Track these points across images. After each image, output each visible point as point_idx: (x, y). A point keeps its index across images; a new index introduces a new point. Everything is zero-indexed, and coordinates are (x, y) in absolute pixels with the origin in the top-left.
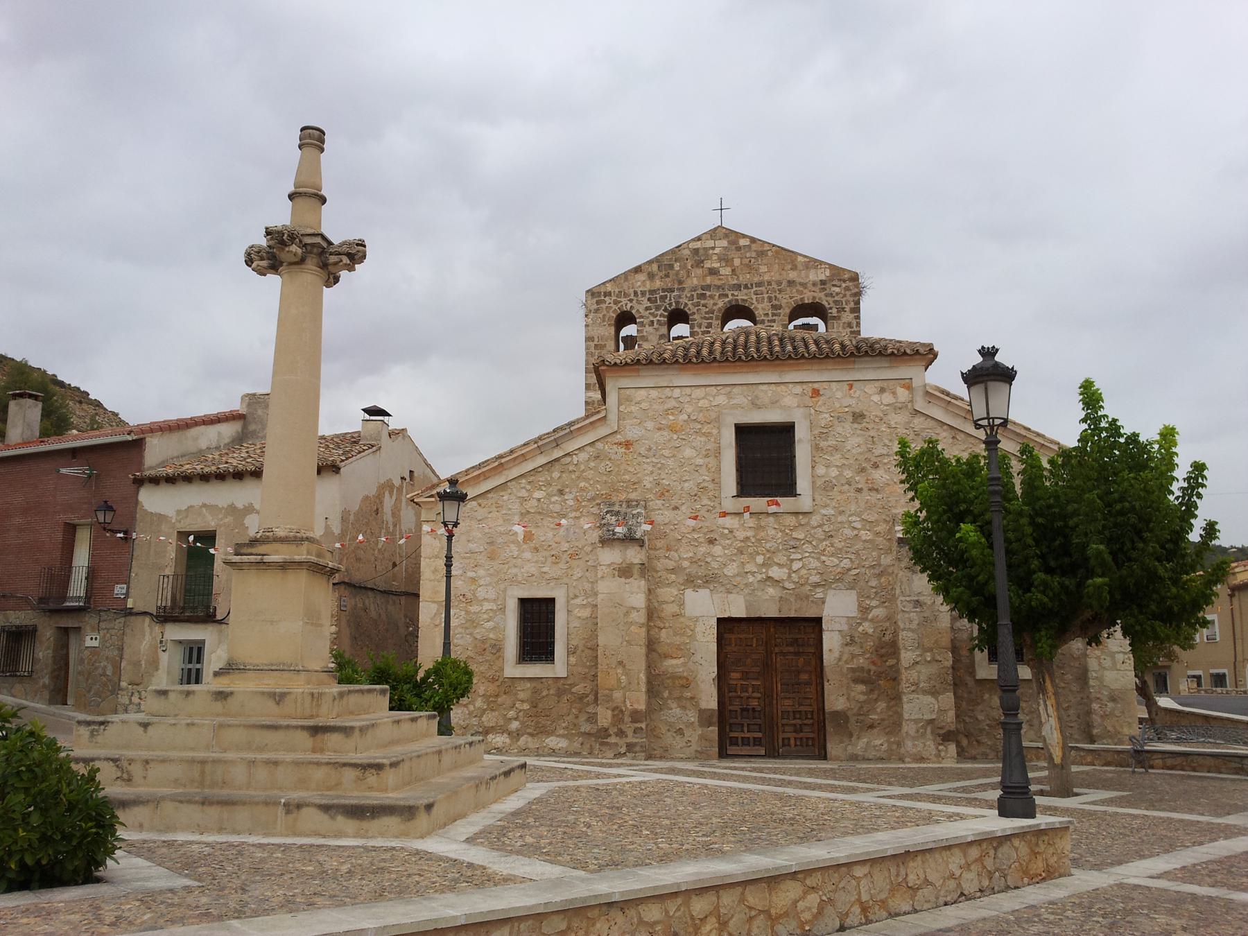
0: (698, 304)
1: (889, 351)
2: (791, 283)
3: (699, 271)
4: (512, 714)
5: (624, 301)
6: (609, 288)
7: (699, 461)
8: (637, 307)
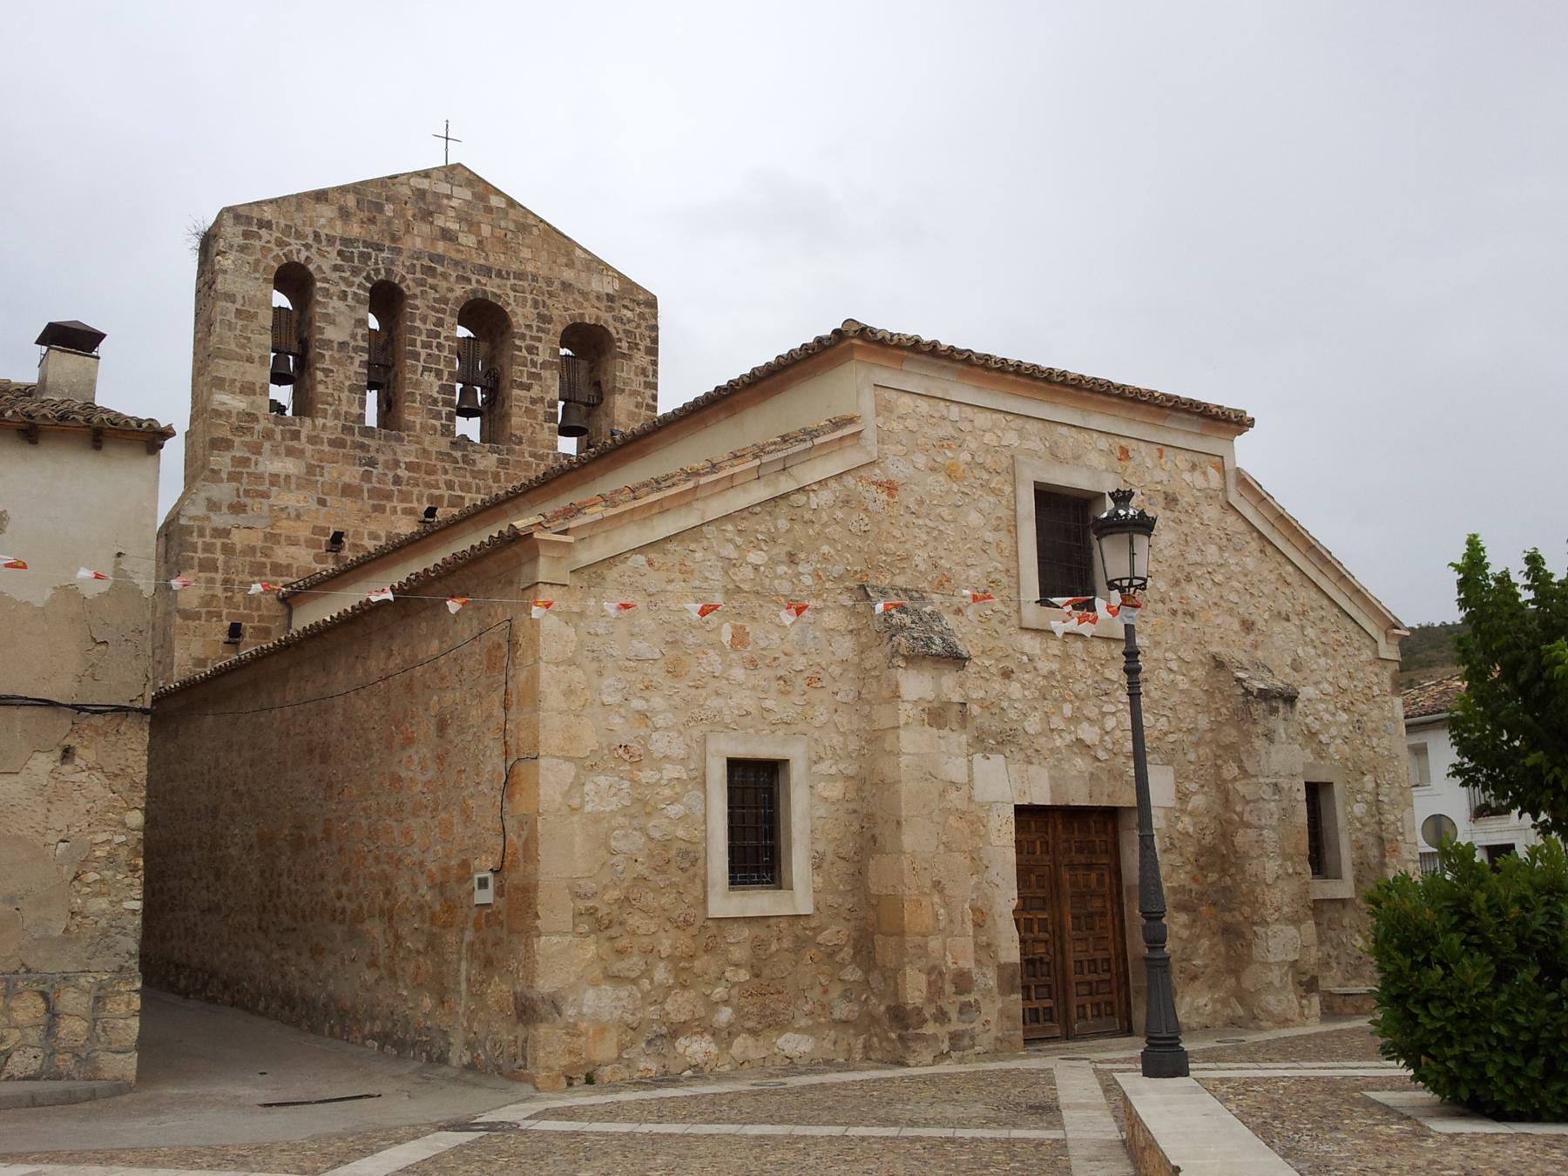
2: (566, 286)
3: (426, 228)
4: (719, 992)
5: (295, 244)
6: (268, 214)
7: (989, 536)
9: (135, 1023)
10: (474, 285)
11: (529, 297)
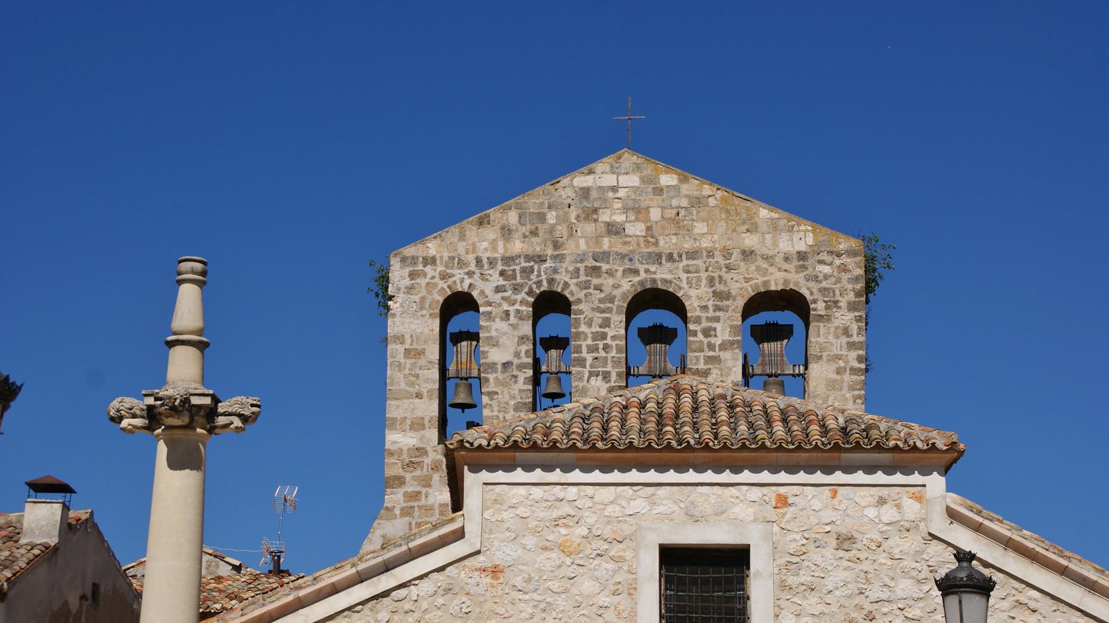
0: (586, 285)
1: (892, 443)
2: (748, 254)
3: (589, 228)
5: (458, 274)
7: (604, 599)
10: (643, 275)
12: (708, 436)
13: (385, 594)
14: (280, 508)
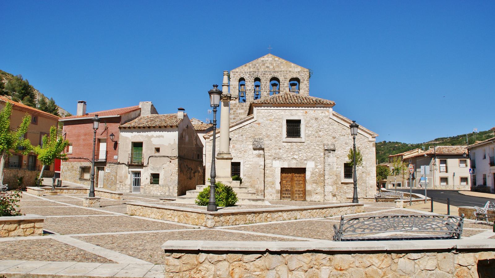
0: (263, 76)
1: (324, 103)
2: (290, 71)
3: (264, 67)
5: (242, 74)
7: (277, 128)
8: (245, 76)
9: (177, 190)
10: (272, 75)
11: (283, 75)
12: (294, 102)
13: (241, 127)
14: (208, 113)
